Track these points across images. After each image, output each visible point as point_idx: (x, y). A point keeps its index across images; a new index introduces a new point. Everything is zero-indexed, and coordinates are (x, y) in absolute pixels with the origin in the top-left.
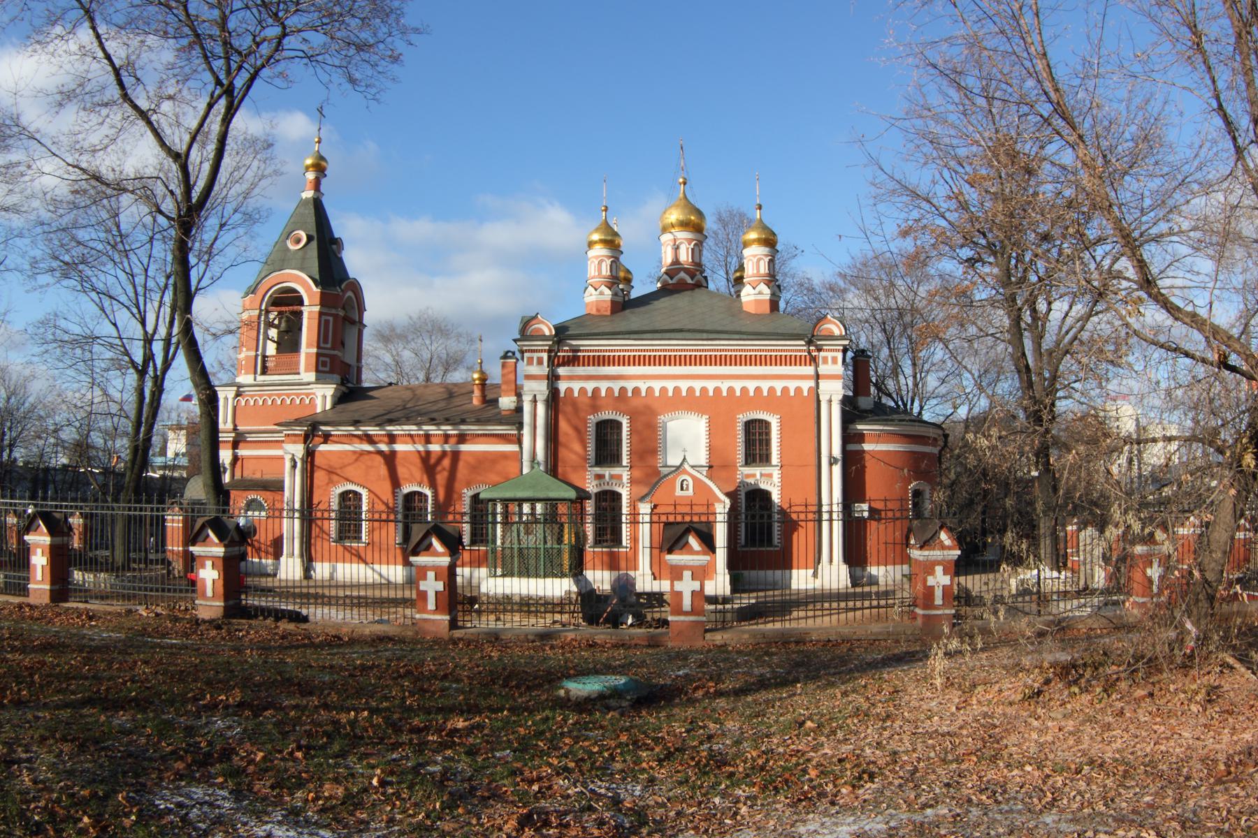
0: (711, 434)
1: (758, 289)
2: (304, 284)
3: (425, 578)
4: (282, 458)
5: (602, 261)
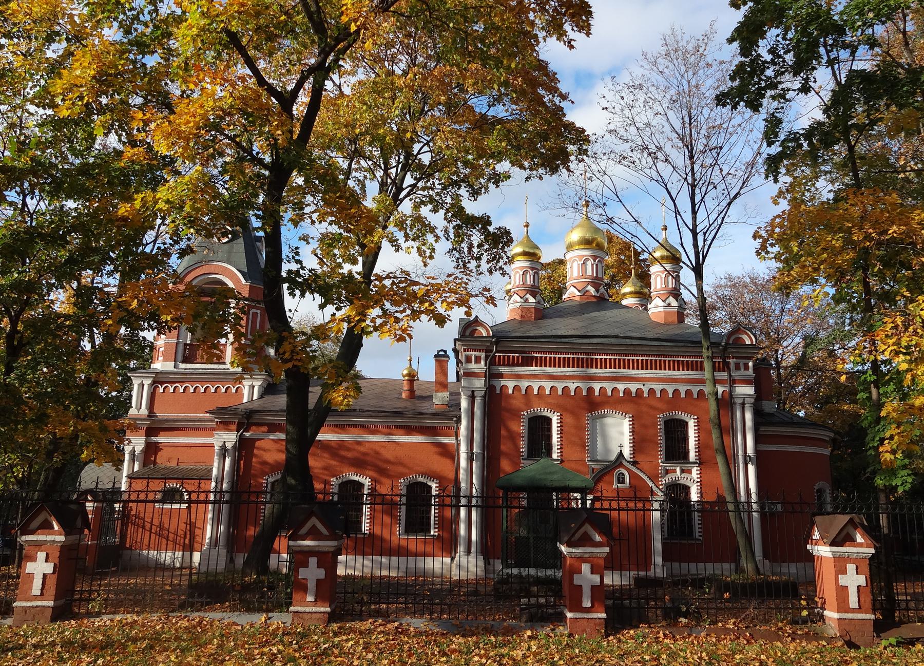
0: (633, 432)
1: (667, 301)
2: (232, 277)
3: (306, 565)
4: (212, 446)
5: (587, 260)
